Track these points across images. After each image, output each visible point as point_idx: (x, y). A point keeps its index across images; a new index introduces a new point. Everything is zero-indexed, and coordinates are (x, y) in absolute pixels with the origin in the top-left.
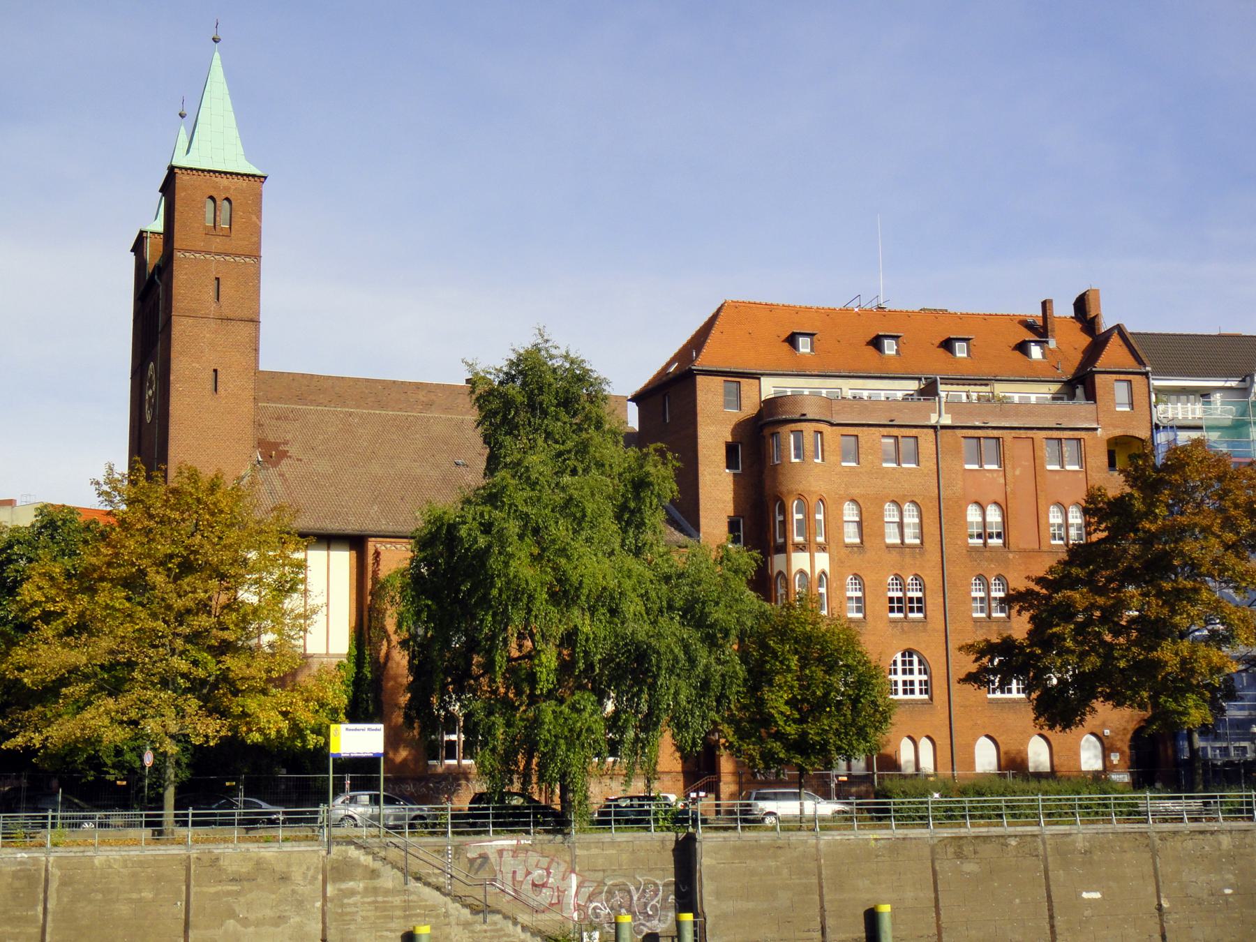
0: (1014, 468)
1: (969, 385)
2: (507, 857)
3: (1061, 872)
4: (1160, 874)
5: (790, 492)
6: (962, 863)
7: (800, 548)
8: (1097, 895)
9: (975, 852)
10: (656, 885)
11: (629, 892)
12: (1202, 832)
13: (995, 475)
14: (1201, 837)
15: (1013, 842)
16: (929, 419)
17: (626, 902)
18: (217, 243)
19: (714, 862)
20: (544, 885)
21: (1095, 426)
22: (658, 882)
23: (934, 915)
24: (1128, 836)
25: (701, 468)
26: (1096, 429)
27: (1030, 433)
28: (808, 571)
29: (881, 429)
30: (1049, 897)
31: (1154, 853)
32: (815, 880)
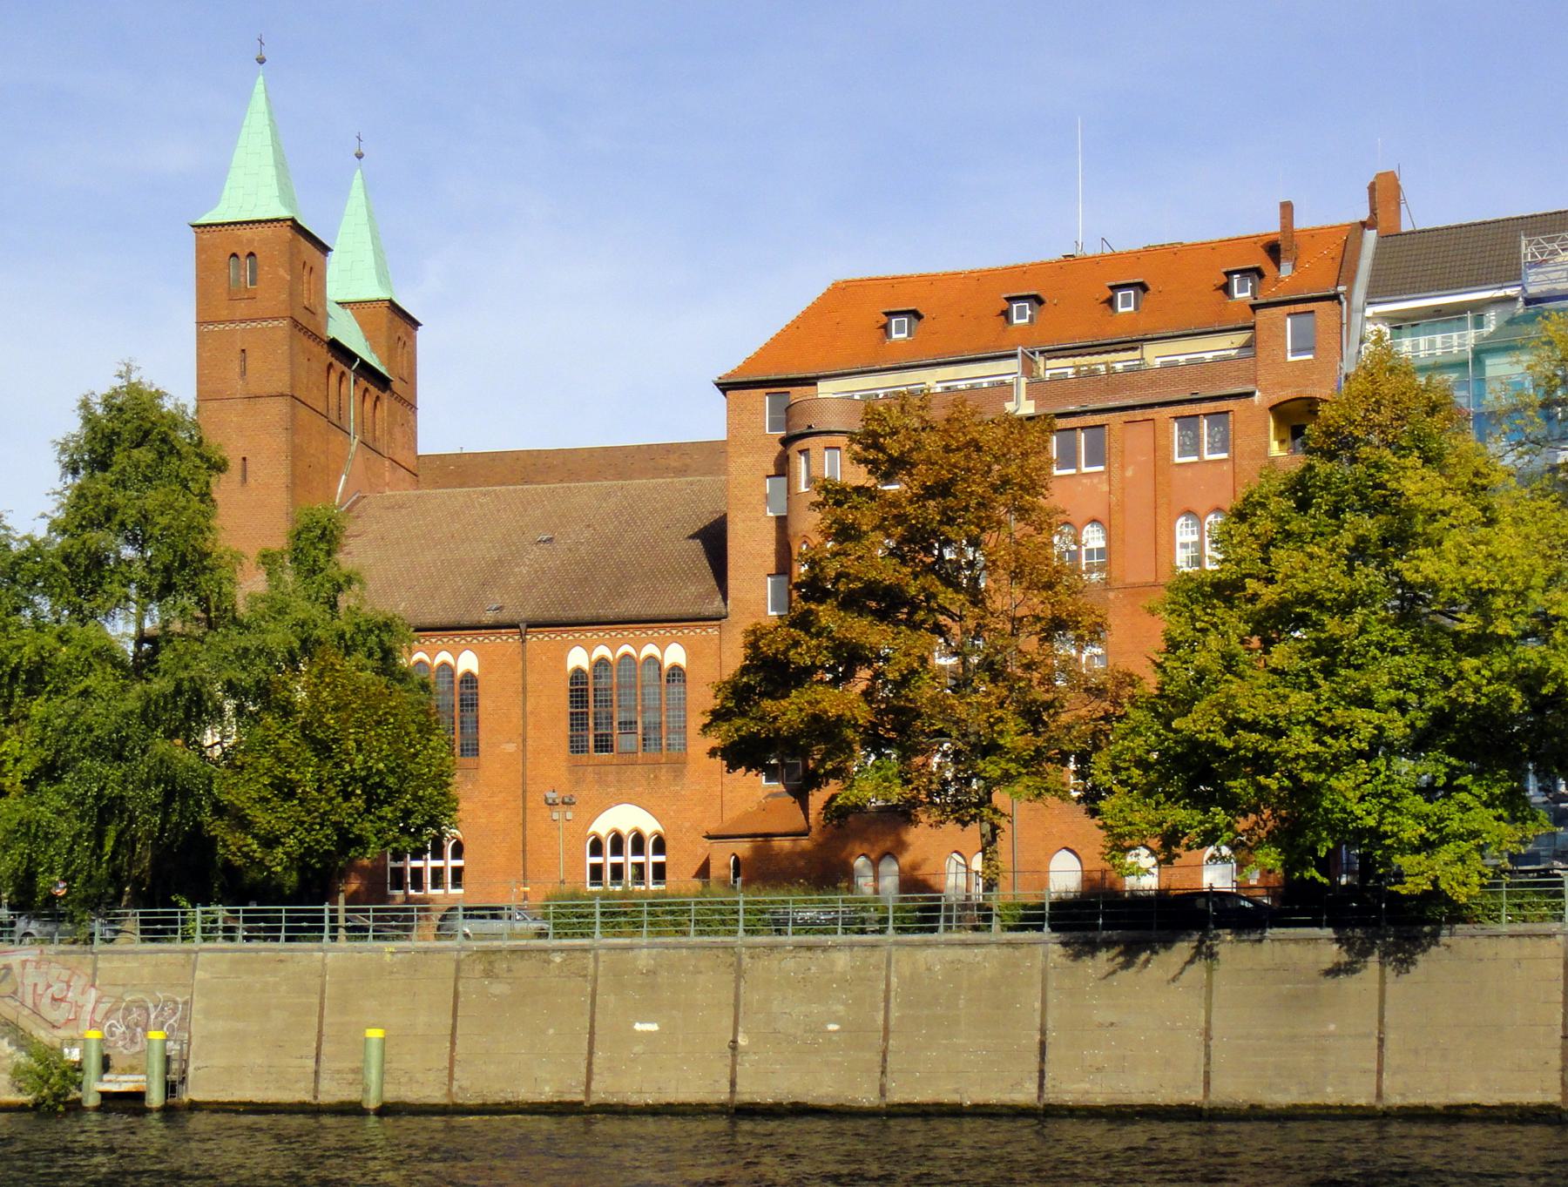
0: (1123, 467)
2: (30, 968)
4: (742, 1003)
5: (796, 534)
6: (491, 983)
8: (654, 1027)
9: (509, 970)
10: (176, 1003)
11: (147, 1009)
12: (809, 948)
13: (1096, 481)
14: (809, 954)
15: (558, 958)
17: (142, 1019)
18: (242, 309)
19: (207, 976)
20: (61, 1000)
21: (1249, 388)
22: (178, 999)
23: (448, 1044)
24: (707, 952)
26: (1251, 394)
27: (1149, 413)
30: (592, 1026)
31: (739, 974)
32: (316, 1000)
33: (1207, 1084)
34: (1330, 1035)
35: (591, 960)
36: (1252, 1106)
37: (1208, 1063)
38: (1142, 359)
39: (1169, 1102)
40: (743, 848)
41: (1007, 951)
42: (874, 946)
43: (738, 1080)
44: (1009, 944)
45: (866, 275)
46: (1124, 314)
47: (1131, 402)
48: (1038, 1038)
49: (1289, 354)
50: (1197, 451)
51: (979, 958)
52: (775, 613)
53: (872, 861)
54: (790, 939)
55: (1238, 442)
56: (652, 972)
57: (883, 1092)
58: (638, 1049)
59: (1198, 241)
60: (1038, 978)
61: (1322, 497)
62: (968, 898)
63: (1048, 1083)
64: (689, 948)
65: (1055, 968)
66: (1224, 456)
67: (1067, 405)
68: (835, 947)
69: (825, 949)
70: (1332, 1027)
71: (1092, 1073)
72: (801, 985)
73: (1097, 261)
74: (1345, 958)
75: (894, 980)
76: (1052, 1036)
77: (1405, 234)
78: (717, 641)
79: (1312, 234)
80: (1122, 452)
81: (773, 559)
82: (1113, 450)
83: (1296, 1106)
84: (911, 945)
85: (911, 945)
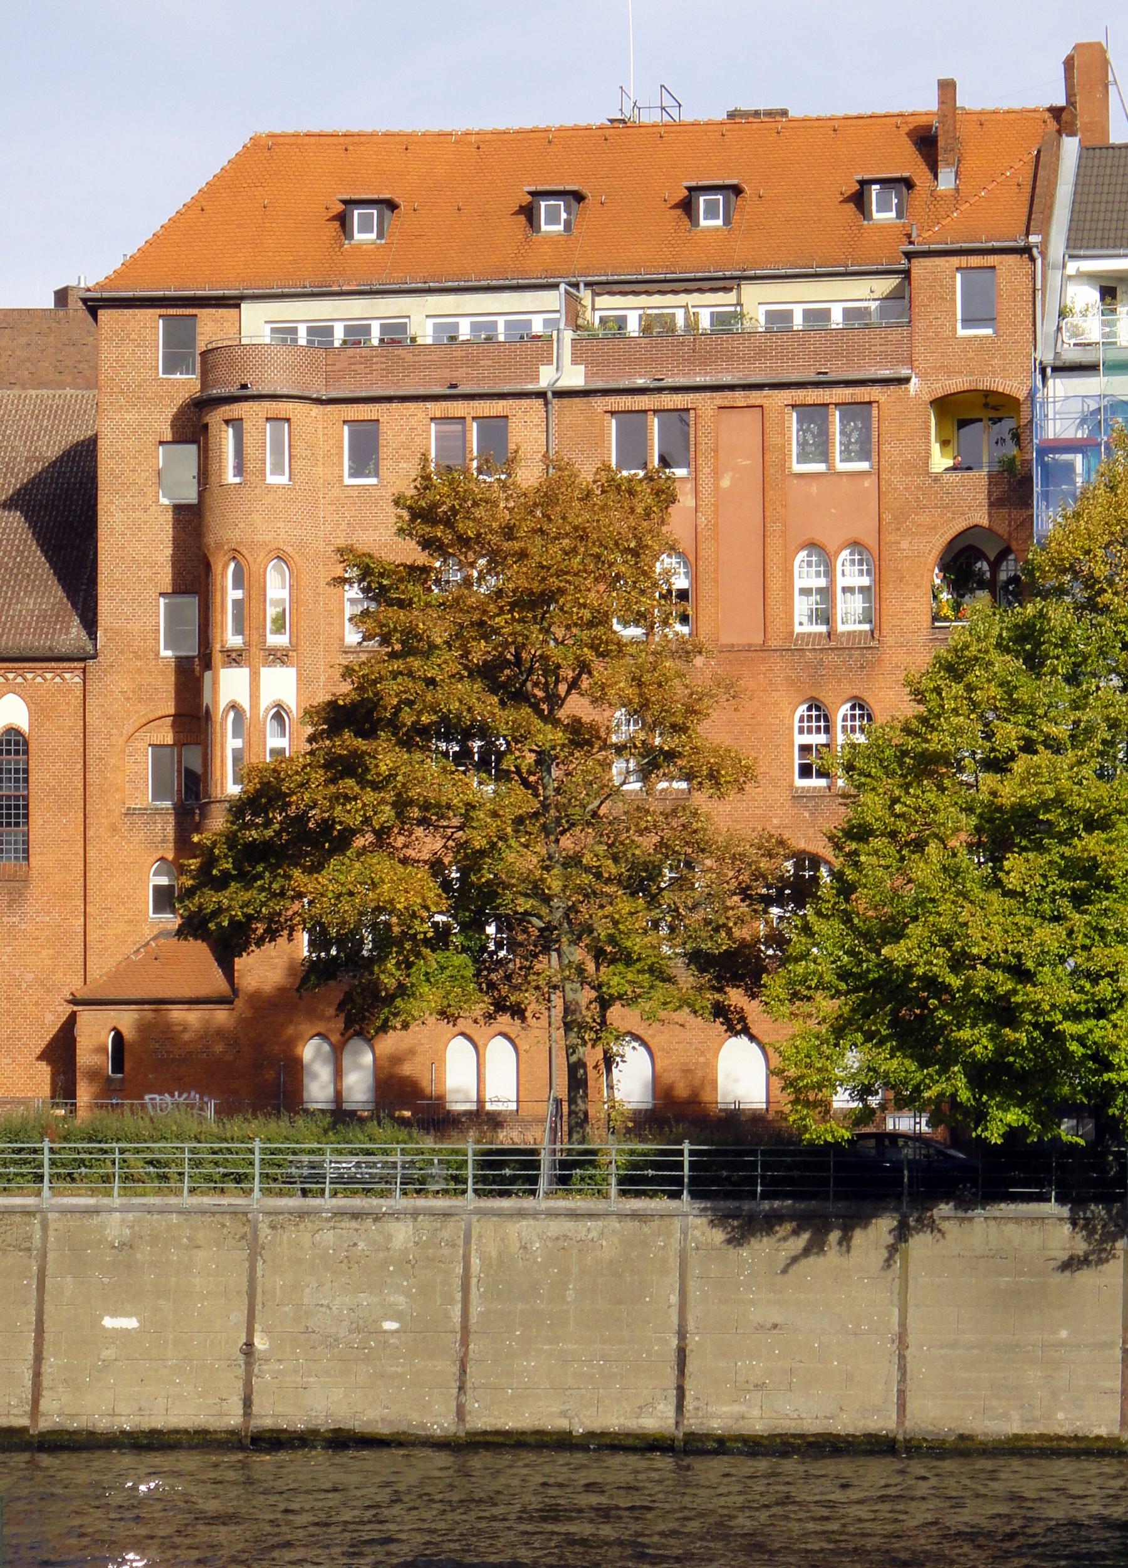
0: (716, 474)
1: (687, 291)
3: (69, 1279)
4: (259, 1290)
5: (219, 546)
7: (235, 658)
8: (131, 1323)
12: (355, 1216)
14: (354, 1224)
16: (536, 378)
21: (904, 372)
24: (208, 1219)
25: (103, 499)
27: (756, 397)
28: (245, 704)
29: (429, 405)
31: (255, 1251)
33: (902, 1407)
34: (1061, 1344)
35: (38, 1227)
36: (962, 1437)
37: (903, 1379)
38: (739, 304)
39: (851, 1430)
40: (126, 1020)
41: (631, 1225)
42: (447, 1215)
43: (256, 1399)
44: (635, 1215)
45: (303, 128)
46: (708, 229)
47: (727, 379)
48: (674, 1342)
49: (959, 325)
50: (824, 456)
51: (594, 1234)
52: (169, 653)
53: (331, 1045)
54: (328, 1203)
55: (885, 448)
56: (127, 1246)
57: (461, 1413)
58: (108, 1353)
59: (814, 114)
60: (674, 1263)
61: (1058, 658)
62: (480, 1101)
63: (689, 1404)
64: (180, 1212)
65: (697, 1248)
66: (864, 466)
67: (631, 375)
68: (395, 1215)
69: (378, 1218)
70: (1064, 1334)
71: (749, 1391)
72: (344, 1266)
73: (661, 133)
74: (1081, 1247)
75: (475, 1262)
76: (694, 1340)
77: (1113, 148)
78: (79, 693)
79: (983, 119)
80: (716, 451)
81: (168, 569)
82: (702, 447)
83: (1017, 1437)
84: (500, 1214)
85: (500, 1214)
